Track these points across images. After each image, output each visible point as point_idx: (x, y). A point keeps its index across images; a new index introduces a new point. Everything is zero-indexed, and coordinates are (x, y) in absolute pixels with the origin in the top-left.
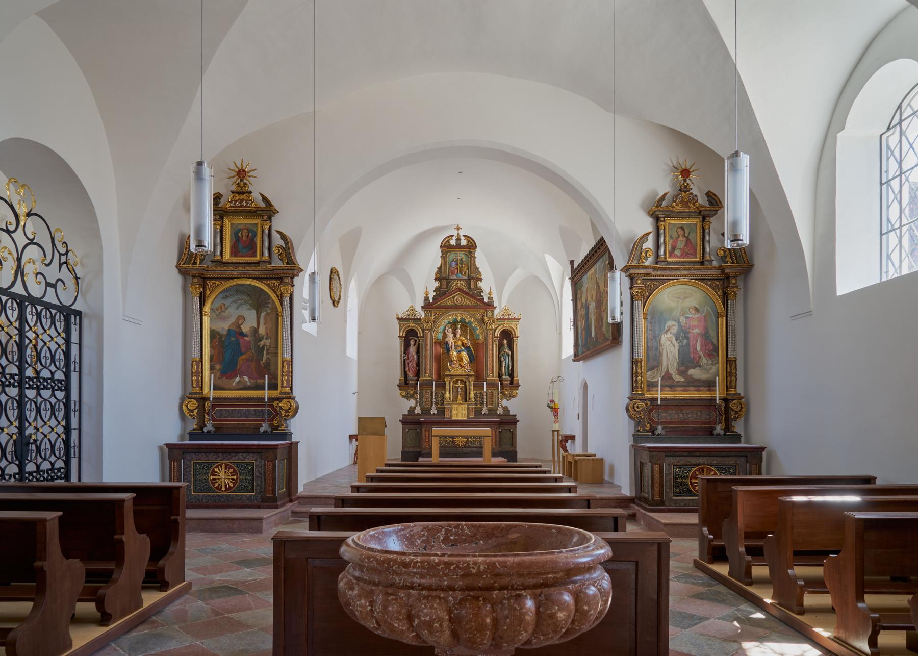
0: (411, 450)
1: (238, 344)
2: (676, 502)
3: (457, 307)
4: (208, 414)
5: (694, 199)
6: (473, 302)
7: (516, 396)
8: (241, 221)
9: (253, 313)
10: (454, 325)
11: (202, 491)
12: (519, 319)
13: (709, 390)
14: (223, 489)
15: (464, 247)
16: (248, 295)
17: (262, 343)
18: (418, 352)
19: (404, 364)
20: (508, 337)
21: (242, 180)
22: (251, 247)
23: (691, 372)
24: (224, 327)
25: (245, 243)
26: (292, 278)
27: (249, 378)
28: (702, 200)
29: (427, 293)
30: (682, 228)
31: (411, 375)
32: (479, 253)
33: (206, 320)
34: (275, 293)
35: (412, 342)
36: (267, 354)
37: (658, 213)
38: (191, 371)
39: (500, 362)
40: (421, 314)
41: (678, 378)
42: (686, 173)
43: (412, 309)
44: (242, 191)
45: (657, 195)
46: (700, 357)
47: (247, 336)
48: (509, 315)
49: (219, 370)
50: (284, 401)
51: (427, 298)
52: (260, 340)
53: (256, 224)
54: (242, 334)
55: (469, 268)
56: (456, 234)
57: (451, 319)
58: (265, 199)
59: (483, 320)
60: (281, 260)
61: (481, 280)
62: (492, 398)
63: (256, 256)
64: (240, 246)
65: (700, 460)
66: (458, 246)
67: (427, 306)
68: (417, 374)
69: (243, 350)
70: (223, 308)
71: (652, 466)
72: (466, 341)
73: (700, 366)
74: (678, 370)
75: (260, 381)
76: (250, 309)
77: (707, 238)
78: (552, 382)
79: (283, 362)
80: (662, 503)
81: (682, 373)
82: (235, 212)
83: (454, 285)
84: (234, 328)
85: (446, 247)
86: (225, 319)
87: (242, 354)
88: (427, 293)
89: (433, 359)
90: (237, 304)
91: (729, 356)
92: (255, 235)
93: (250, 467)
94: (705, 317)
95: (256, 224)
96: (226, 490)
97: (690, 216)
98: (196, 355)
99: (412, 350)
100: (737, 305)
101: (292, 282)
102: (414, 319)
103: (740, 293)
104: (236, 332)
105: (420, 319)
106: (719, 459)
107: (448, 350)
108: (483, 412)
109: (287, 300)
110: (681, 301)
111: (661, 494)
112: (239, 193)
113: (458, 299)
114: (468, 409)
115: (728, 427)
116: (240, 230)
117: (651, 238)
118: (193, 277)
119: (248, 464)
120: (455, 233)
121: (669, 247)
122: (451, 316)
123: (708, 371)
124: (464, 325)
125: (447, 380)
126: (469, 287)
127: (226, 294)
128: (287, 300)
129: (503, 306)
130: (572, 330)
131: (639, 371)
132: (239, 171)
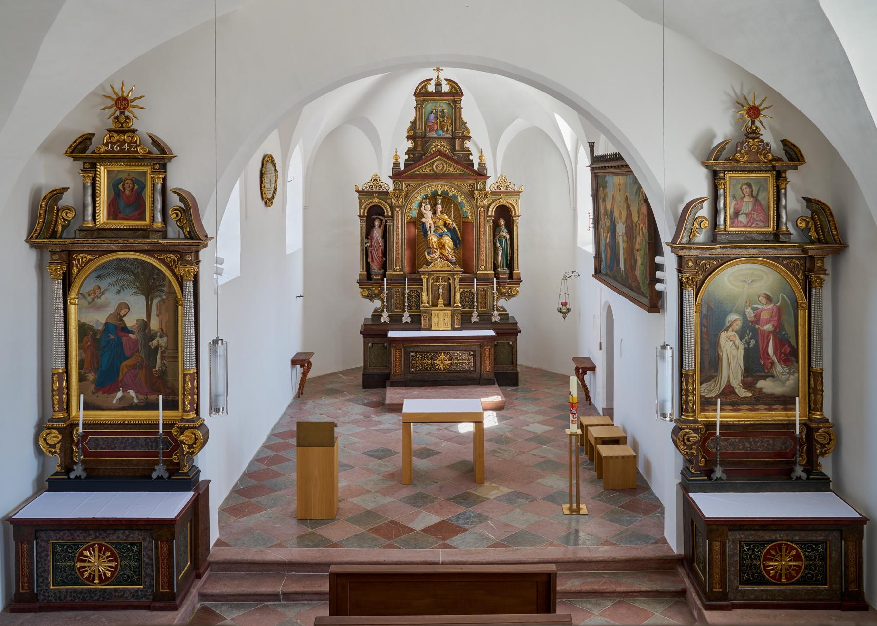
0: (375, 371)
1: (120, 344)
2: (744, 593)
3: (436, 176)
4: (77, 445)
5: (765, 148)
6: (459, 169)
7: (516, 295)
8: (121, 168)
9: (141, 300)
10: (433, 199)
11: (65, 584)
12: (520, 192)
13: (785, 410)
14: (96, 581)
15: (445, 94)
16: (134, 274)
17: (154, 343)
18: (384, 236)
19: (366, 253)
20: (505, 215)
21: (122, 113)
22: (137, 207)
23: (761, 384)
24: (98, 319)
25: (128, 200)
26: (197, 252)
27: (137, 392)
28: (776, 148)
29: (396, 157)
30: (749, 185)
31: (375, 268)
32: (466, 102)
33: (72, 309)
34: (173, 271)
35: (377, 223)
36: (162, 358)
37: (717, 162)
38: (53, 390)
39: (495, 250)
40: (389, 184)
41: (743, 393)
42: (754, 112)
43: (376, 179)
44: (122, 127)
45: (713, 136)
46: (773, 363)
47: (133, 332)
48: (507, 187)
49: (93, 382)
50: (186, 433)
51: (396, 165)
52: (152, 338)
53: (145, 173)
54: (125, 330)
55: (453, 123)
56: (435, 78)
57: (429, 192)
58: (155, 142)
59: (472, 194)
60: (181, 227)
61: (469, 138)
62: (485, 298)
63: (144, 218)
64: (122, 204)
65: (777, 535)
66: (438, 93)
67: (397, 175)
68: (384, 266)
69: (127, 352)
70: (98, 292)
71: (710, 545)
72: (449, 221)
73: (773, 376)
74: (743, 382)
75: (152, 397)
76: (136, 294)
77: (784, 203)
78: (565, 278)
79: (185, 375)
80: (724, 596)
81: (747, 385)
82: (111, 158)
83: (433, 148)
84: (113, 321)
85: (422, 94)
86: (99, 308)
87: (126, 358)
88: (396, 157)
89: (405, 247)
90: (118, 287)
91: (813, 365)
92: (143, 187)
93: (135, 549)
94: (779, 309)
95: (145, 173)
96: (102, 581)
97: (759, 171)
98: (59, 365)
99: (377, 233)
100: (824, 294)
101: (197, 257)
102: (379, 193)
103: (828, 279)
104: (116, 327)
105: (387, 192)
106: (803, 534)
107: (425, 232)
108: (473, 320)
109: (190, 285)
110: (747, 284)
111: (723, 585)
112: (118, 132)
113: (439, 165)
114: (452, 316)
115: (811, 466)
116: (121, 181)
117: (706, 205)
118: (53, 252)
119: (132, 544)
120: (433, 75)
121: (730, 211)
122: (428, 188)
123: (783, 383)
124: (447, 199)
125: (424, 278)
126: (453, 149)
127: (102, 272)
128: (190, 285)
129: (499, 175)
130: (592, 230)
131: (691, 388)
132: (119, 99)
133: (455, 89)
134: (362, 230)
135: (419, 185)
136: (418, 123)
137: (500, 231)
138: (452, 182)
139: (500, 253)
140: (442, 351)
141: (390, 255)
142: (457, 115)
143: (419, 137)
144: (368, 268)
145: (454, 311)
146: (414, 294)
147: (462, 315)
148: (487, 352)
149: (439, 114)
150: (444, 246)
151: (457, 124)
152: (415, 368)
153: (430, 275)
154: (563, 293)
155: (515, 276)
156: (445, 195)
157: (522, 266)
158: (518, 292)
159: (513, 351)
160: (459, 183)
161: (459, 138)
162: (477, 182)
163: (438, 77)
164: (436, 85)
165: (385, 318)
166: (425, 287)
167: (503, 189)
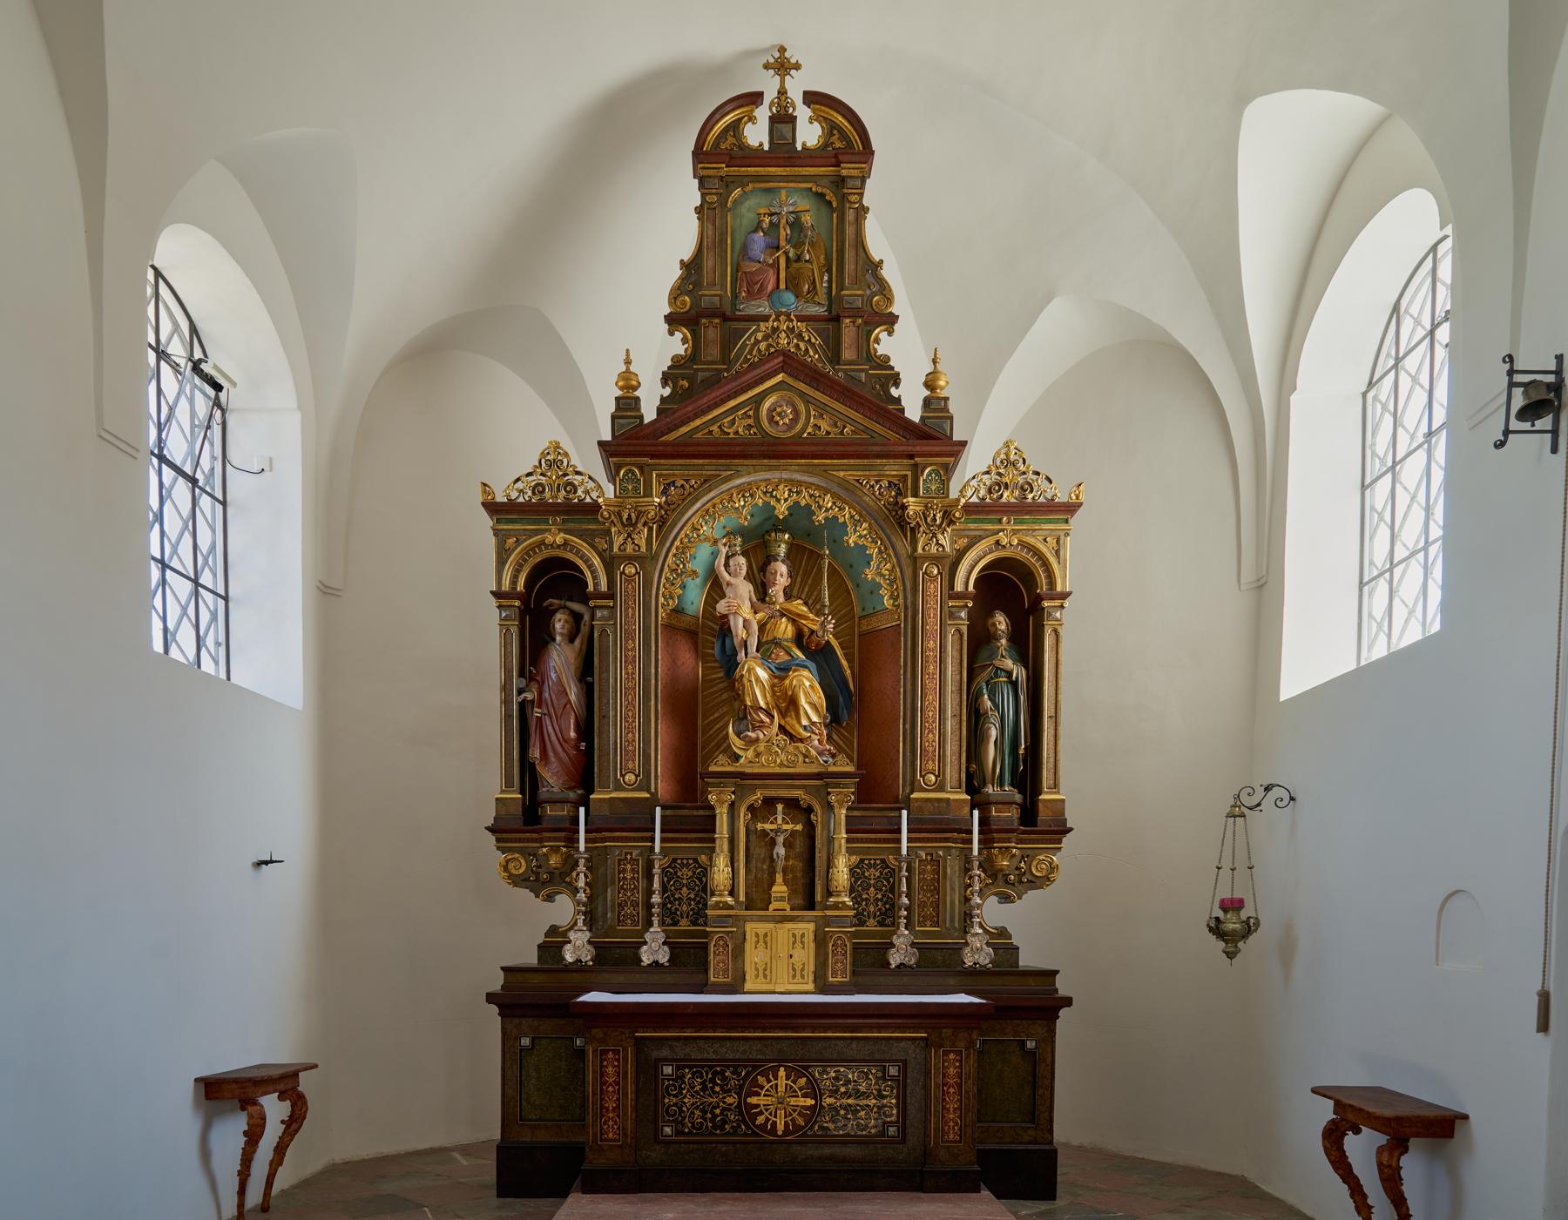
0: (542, 1137)
6: (850, 423)
7: (1045, 881)
15: (809, 157)
18: (586, 670)
19: (523, 725)
20: (1015, 600)
29: (628, 382)
31: (552, 779)
35: (560, 623)
51: (627, 405)
56: (770, 95)
57: (743, 511)
66: (783, 150)
68: (584, 776)
72: (812, 622)
78: (1237, 812)
88: (628, 382)
105: (595, 508)
107: (730, 663)
108: (895, 959)
113: (777, 406)
114: (821, 940)
125: (722, 800)
133: (844, 136)
134: (506, 645)
135: (708, 482)
136: (708, 262)
137: (993, 654)
138: (825, 472)
139: (994, 733)
140: (781, 1061)
141: (604, 733)
142: (850, 231)
143: (712, 313)
144: (528, 776)
145: (828, 921)
146: (685, 873)
147: (856, 947)
148: (951, 1067)
149: (785, 232)
150: (793, 703)
151: (849, 267)
152: (678, 1123)
153: (741, 792)
154: (1227, 864)
155: (1043, 814)
156: (800, 526)
157: (1072, 782)
158: (1053, 868)
159: (1038, 1075)
160: (850, 475)
161: (855, 313)
162: (917, 470)
163: (782, 92)
164: (774, 120)
165: (578, 948)
166: (722, 845)
167: (1007, 496)
